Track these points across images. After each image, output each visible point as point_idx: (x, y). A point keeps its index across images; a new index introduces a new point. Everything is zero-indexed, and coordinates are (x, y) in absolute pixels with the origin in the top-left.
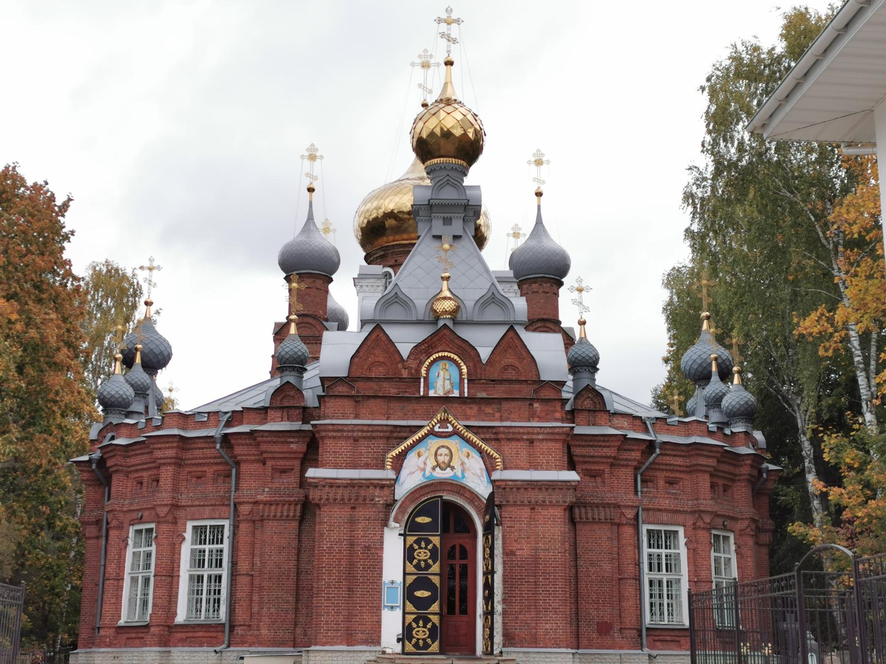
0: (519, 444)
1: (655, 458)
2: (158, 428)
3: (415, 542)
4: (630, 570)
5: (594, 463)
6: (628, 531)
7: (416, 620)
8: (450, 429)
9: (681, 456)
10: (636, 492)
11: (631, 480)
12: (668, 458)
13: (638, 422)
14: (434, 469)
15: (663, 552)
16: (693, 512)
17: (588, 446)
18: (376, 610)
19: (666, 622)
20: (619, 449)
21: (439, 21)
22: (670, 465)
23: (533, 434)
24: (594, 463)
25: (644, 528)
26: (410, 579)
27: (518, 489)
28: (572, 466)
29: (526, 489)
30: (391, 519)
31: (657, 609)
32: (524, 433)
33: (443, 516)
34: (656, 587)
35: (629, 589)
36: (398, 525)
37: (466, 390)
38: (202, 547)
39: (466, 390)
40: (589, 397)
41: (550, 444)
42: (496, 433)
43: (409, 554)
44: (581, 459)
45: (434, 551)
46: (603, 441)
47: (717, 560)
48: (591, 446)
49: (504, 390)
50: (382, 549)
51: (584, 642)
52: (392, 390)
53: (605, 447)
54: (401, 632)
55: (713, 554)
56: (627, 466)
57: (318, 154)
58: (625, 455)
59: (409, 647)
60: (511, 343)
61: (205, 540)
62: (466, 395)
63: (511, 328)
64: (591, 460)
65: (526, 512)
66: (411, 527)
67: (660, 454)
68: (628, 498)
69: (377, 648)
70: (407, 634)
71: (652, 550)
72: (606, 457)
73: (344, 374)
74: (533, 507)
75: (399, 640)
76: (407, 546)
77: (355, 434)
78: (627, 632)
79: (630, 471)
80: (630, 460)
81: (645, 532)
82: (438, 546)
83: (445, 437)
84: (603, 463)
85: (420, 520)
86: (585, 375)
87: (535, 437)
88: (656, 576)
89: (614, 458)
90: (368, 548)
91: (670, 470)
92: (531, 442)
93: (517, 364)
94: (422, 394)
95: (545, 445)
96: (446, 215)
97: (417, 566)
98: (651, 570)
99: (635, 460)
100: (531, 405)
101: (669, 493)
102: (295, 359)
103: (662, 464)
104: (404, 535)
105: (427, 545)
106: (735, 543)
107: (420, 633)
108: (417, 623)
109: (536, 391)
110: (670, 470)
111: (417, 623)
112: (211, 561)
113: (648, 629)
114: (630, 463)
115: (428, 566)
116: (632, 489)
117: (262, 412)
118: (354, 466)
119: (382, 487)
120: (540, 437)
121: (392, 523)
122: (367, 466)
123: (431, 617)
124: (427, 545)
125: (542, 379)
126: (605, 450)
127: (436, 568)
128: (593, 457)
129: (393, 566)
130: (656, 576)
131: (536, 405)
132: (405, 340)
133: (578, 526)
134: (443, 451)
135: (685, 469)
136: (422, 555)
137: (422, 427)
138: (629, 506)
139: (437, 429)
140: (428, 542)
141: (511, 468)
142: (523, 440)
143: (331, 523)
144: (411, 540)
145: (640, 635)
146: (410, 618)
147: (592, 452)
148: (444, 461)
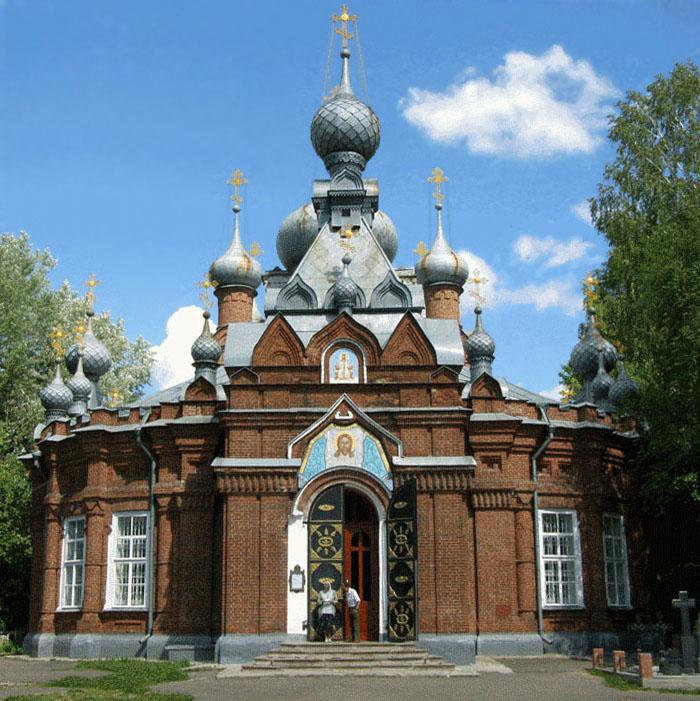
0: (418, 431)
2: (87, 424)
4: (527, 554)
6: (527, 515)
8: (351, 416)
10: (531, 477)
13: (532, 409)
14: (351, 455)
18: (282, 598)
25: (540, 513)
26: (315, 566)
28: (469, 450)
33: (348, 505)
35: (527, 572)
36: (301, 513)
37: (365, 377)
38: (127, 537)
39: (365, 377)
43: (313, 541)
45: (337, 539)
47: (609, 542)
49: (407, 383)
50: (287, 537)
51: (483, 625)
52: (294, 378)
54: (306, 619)
55: (604, 537)
60: (410, 328)
61: (145, 530)
62: (366, 382)
63: (409, 313)
66: (315, 515)
67: (553, 440)
68: (521, 482)
69: (278, 637)
73: (246, 364)
75: (304, 629)
76: (311, 534)
77: (259, 424)
81: (540, 517)
82: (341, 532)
85: (322, 507)
88: (552, 558)
89: (510, 444)
93: (415, 351)
94: (323, 382)
96: (344, 207)
97: (321, 554)
98: (546, 553)
100: (429, 391)
102: (208, 355)
104: (309, 523)
105: (330, 532)
109: (435, 377)
112: (135, 550)
113: (544, 612)
116: (528, 474)
117: (179, 407)
119: (286, 476)
121: (296, 512)
122: (271, 455)
124: (330, 532)
125: (439, 363)
126: (501, 436)
127: (339, 555)
131: (434, 390)
132: (306, 327)
133: (477, 513)
134: (345, 439)
136: (326, 541)
137: (323, 414)
138: (524, 492)
139: (337, 417)
140: (331, 529)
142: (421, 426)
143: (239, 515)
144: (314, 528)
145: (537, 617)
147: (489, 439)
148: (344, 448)
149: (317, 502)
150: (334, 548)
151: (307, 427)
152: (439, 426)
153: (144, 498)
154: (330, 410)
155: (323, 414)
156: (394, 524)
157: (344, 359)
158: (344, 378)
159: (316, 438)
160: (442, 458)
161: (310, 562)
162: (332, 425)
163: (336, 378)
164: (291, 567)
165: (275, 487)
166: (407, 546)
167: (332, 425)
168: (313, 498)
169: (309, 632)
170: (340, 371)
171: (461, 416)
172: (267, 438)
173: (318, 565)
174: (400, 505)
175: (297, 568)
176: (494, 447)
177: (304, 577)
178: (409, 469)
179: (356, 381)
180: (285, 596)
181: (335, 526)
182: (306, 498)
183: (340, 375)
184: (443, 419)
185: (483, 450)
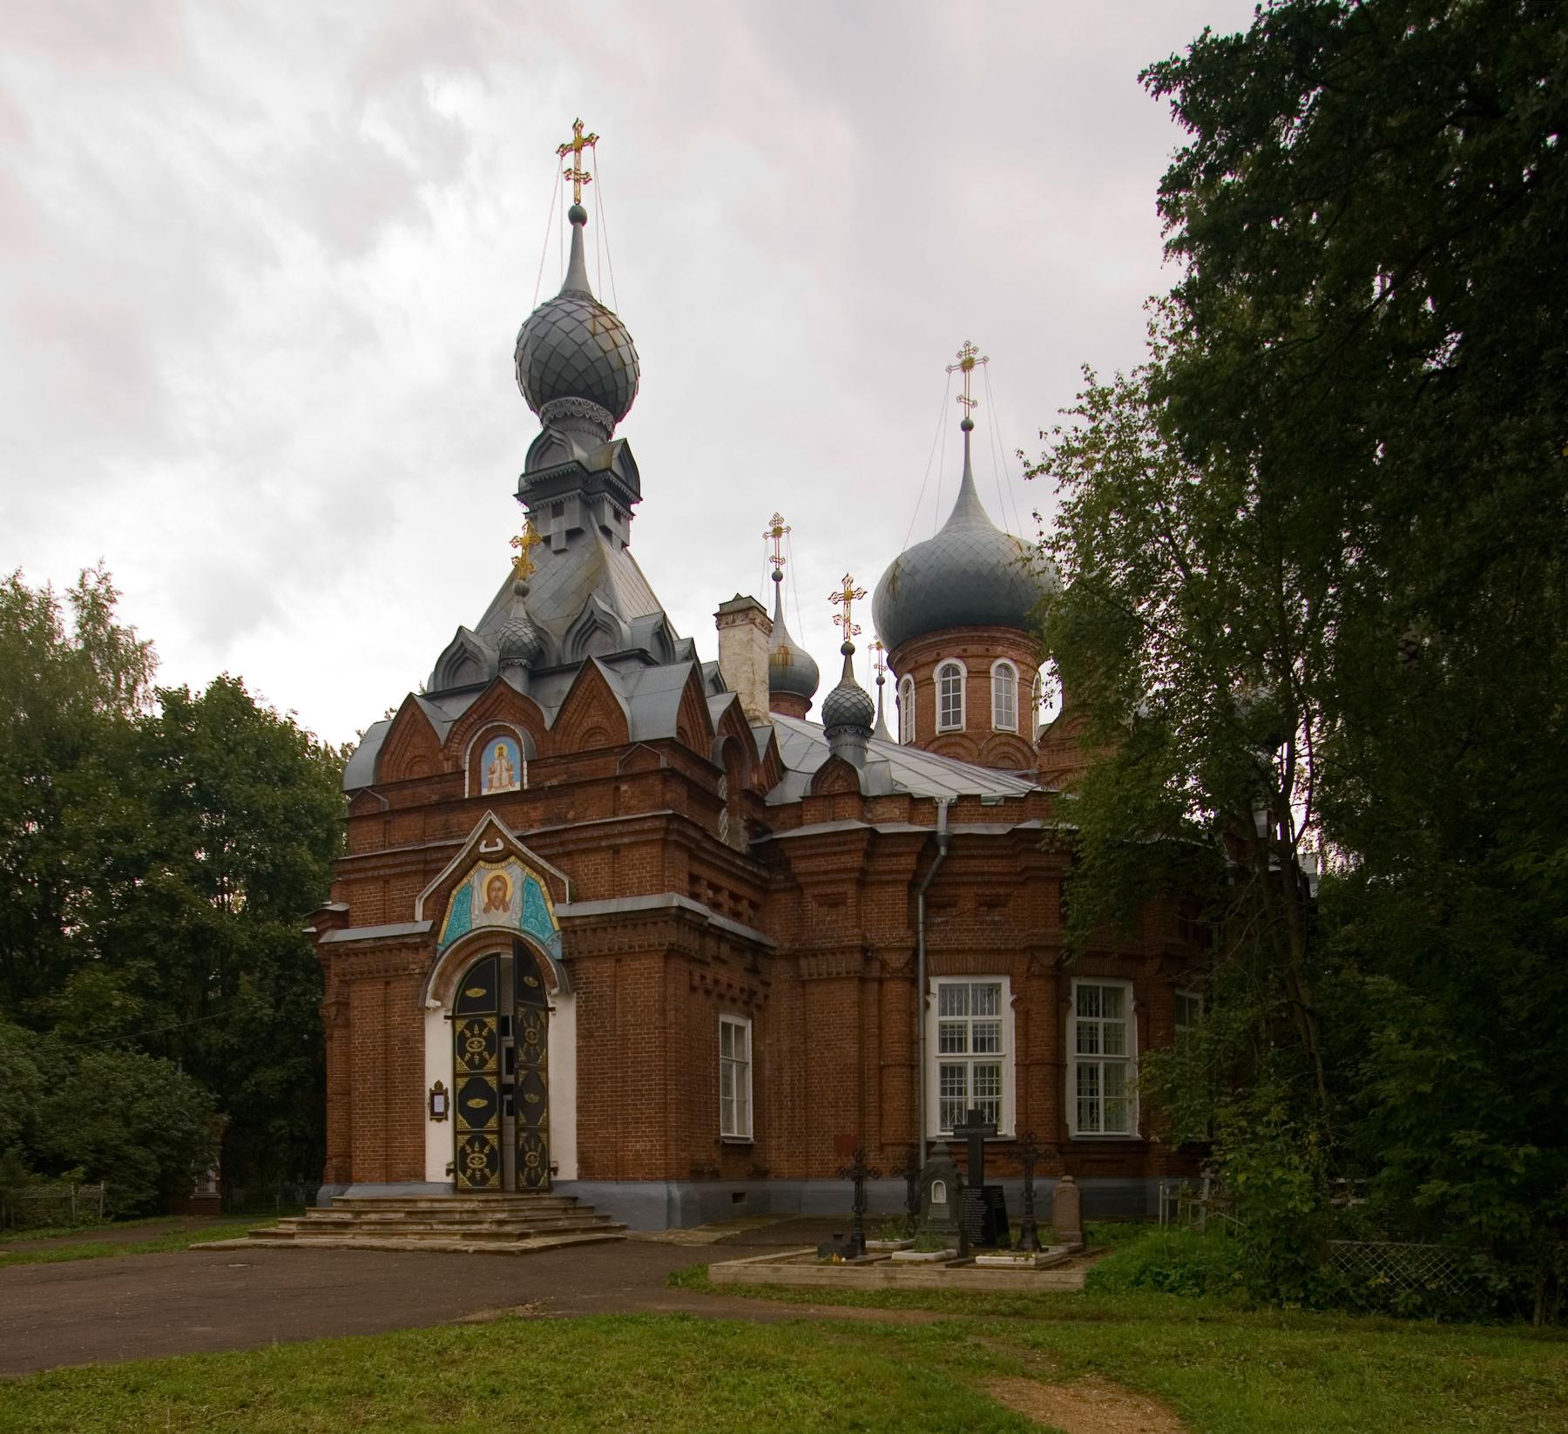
1: (941, 866)
3: (467, 1027)
5: (831, 882)
7: (470, 1142)
8: (501, 846)
9: (1003, 857)
11: (902, 906)
12: (977, 862)
14: (486, 910)
15: (1101, 1021)
16: (1024, 951)
17: (817, 855)
19: (1102, 1133)
20: (868, 855)
21: (563, 150)
22: (983, 874)
23: (614, 836)
24: (831, 882)
26: (462, 1082)
27: (594, 930)
29: (605, 929)
30: (429, 995)
31: (1086, 1111)
32: (600, 838)
33: (502, 989)
34: (1086, 1079)
36: (438, 1004)
40: (838, 777)
41: (644, 850)
42: (562, 844)
44: (809, 879)
46: (839, 844)
48: (823, 855)
50: (423, 1041)
53: (843, 853)
56: (895, 882)
57: (783, 526)
58: (882, 865)
59: (464, 1181)
64: (825, 878)
65: (608, 967)
70: (459, 1163)
71: (1082, 1019)
72: (846, 870)
74: (619, 957)
75: (448, 1172)
78: (889, 1149)
79: (901, 892)
80: (898, 872)
83: (498, 861)
84: (844, 881)
86: (848, 738)
87: (618, 841)
90: (406, 1040)
91: (986, 883)
92: (616, 850)
95: (636, 854)
97: (470, 1063)
99: (906, 871)
101: (982, 923)
103: (966, 874)
104: (453, 1019)
106: (1136, 998)
107: (477, 1161)
108: (472, 1147)
109: (626, 764)
110: (986, 883)
111: (472, 1147)
114: (899, 877)
115: (484, 1062)
118: (385, 920)
120: (626, 840)
123: (489, 1137)
128: (826, 873)
129: (439, 1060)
130: (953, 1058)
131: (624, 788)
134: (497, 884)
135: (1015, 879)
136: (476, 1045)
137: (462, 845)
139: (482, 849)
140: (483, 1025)
141: (588, 899)
144: (460, 1025)
146: (463, 1139)
147: (823, 864)
149: (466, 984)
150: (486, 1054)
151: (438, 871)
152: (631, 845)
153: (851, 949)
154: (469, 842)
155: (462, 845)
156: (465, 1022)
157: (501, 754)
158: (501, 786)
159: (458, 887)
160: (629, 900)
161: (456, 1075)
162: (481, 863)
163: (491, 787)
164: (430, 1085)
165: (399, 964)
166: (486, 1054)
167: (481, 863)
168: (457, 978)
169: (456, 1178)
170: (496, 775)
171: (658, 823)
172: (396, 895)
173: (466, 1080)
174: (475, 993)
175: (439, 1085)
176: (820, 878)
177: (446, 1099)
178: (578, 922)
179: (517, 788)
180: (422, 1128)
181: (487, 1020)
182: (444, 978)
183: (496, 783)
184: (635, 833)
185: (817, 883)
